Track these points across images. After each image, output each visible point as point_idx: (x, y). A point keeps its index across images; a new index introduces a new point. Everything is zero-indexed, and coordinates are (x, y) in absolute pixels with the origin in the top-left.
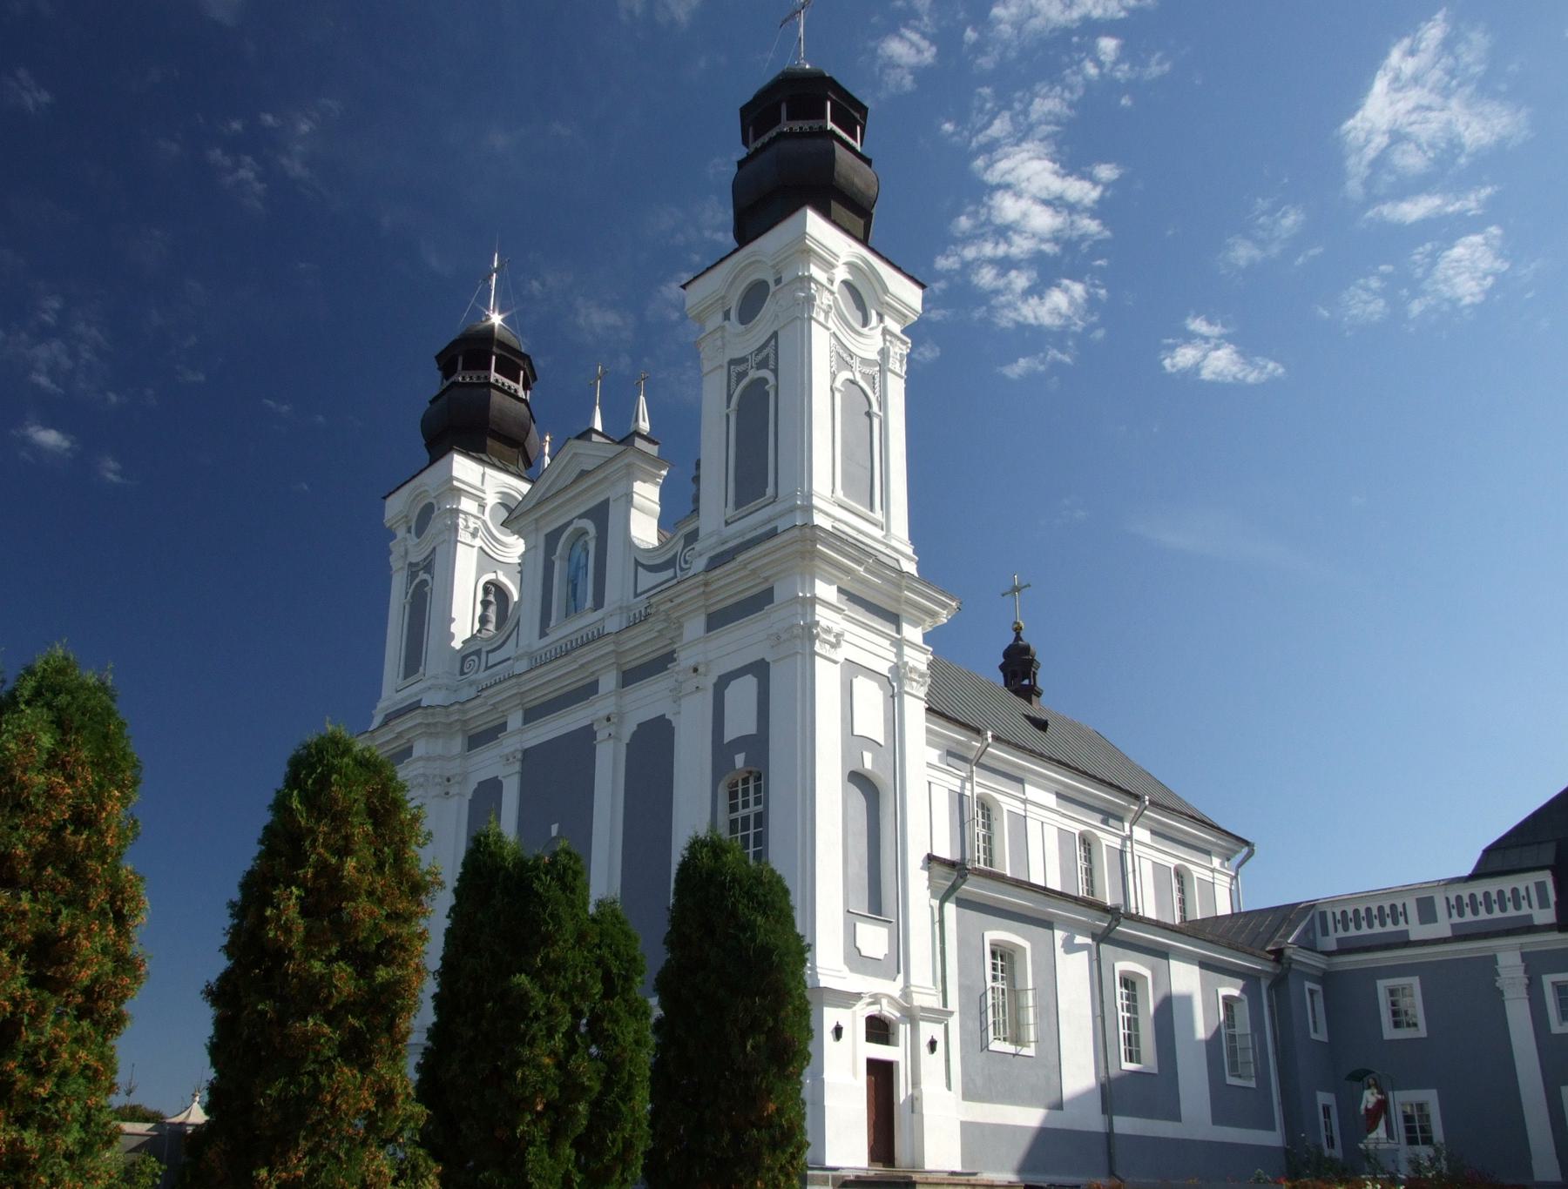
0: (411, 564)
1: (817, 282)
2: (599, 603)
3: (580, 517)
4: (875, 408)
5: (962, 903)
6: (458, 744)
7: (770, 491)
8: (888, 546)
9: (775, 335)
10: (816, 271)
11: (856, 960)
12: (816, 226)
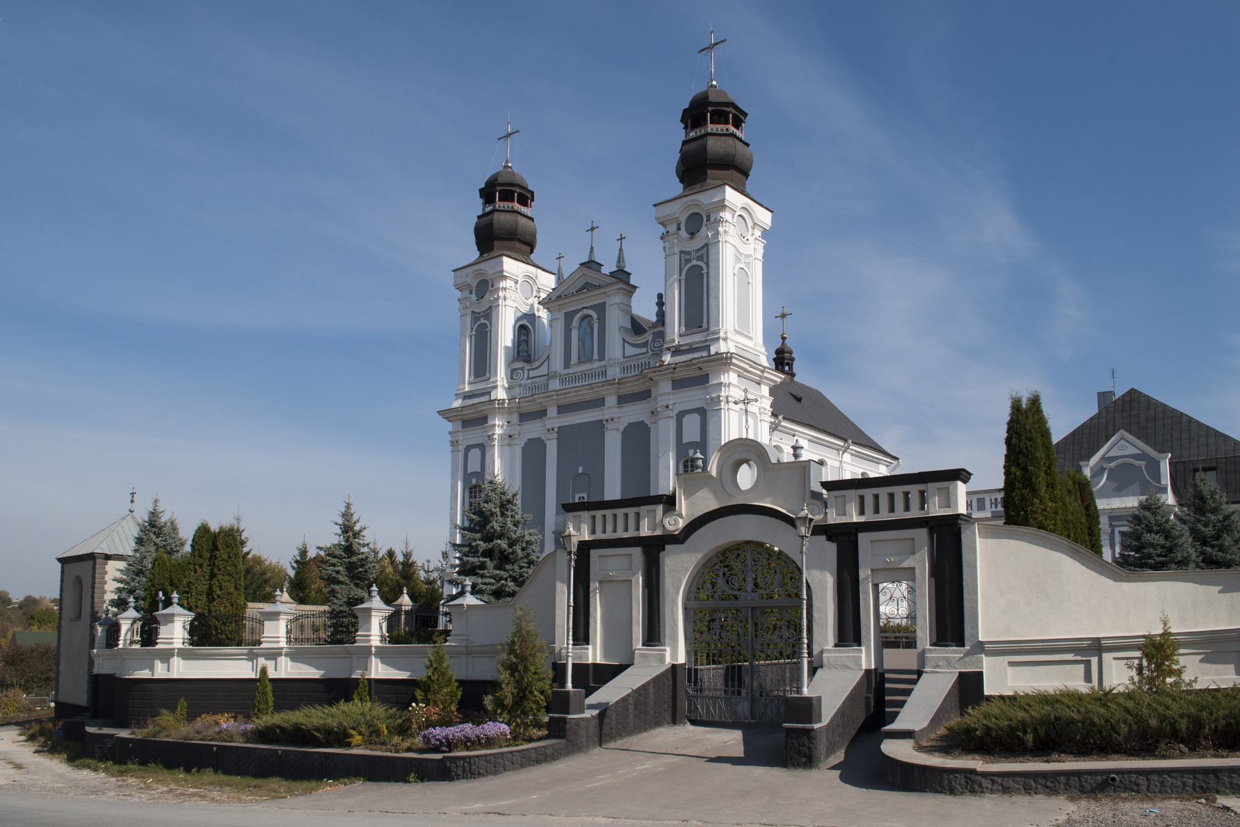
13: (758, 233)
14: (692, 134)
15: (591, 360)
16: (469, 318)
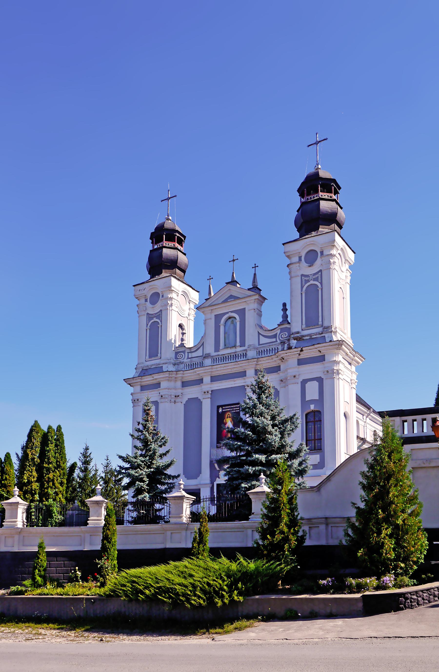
3: (231, 312)
6: (179, 384)
7: (159, 355)
13: (347, 266)
14: (156, 247)
15: (235, 346)
16: (144, 318)
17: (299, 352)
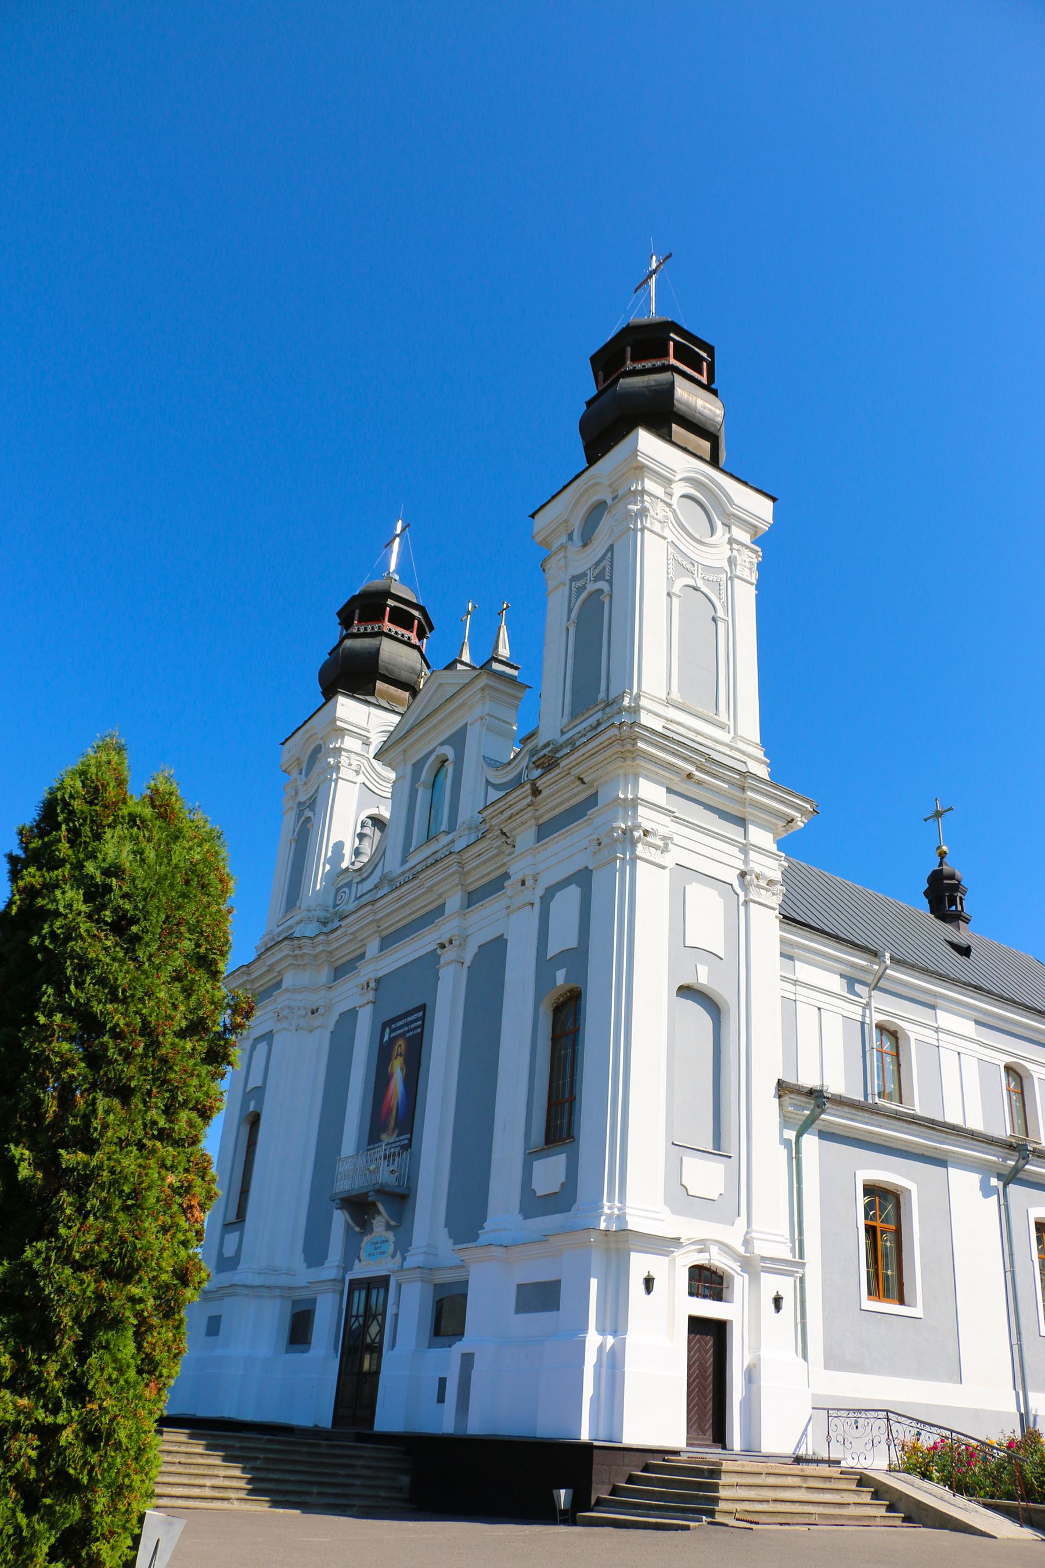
0: (300, 804)
1: (650, 495)
2: (452, 828)
3: (442, 744)
4: (721, 613)
5: (823, 1135)
6: (324, 975)
8: (731, 748)
9: (611, 548)
10: (650, 485)
11: (682, 1198)
12: (646, 441)
17: (529, 799)
